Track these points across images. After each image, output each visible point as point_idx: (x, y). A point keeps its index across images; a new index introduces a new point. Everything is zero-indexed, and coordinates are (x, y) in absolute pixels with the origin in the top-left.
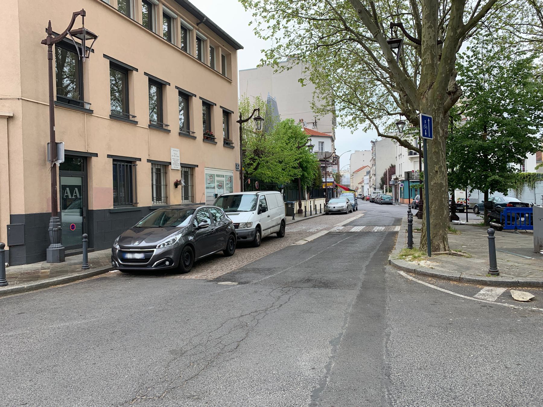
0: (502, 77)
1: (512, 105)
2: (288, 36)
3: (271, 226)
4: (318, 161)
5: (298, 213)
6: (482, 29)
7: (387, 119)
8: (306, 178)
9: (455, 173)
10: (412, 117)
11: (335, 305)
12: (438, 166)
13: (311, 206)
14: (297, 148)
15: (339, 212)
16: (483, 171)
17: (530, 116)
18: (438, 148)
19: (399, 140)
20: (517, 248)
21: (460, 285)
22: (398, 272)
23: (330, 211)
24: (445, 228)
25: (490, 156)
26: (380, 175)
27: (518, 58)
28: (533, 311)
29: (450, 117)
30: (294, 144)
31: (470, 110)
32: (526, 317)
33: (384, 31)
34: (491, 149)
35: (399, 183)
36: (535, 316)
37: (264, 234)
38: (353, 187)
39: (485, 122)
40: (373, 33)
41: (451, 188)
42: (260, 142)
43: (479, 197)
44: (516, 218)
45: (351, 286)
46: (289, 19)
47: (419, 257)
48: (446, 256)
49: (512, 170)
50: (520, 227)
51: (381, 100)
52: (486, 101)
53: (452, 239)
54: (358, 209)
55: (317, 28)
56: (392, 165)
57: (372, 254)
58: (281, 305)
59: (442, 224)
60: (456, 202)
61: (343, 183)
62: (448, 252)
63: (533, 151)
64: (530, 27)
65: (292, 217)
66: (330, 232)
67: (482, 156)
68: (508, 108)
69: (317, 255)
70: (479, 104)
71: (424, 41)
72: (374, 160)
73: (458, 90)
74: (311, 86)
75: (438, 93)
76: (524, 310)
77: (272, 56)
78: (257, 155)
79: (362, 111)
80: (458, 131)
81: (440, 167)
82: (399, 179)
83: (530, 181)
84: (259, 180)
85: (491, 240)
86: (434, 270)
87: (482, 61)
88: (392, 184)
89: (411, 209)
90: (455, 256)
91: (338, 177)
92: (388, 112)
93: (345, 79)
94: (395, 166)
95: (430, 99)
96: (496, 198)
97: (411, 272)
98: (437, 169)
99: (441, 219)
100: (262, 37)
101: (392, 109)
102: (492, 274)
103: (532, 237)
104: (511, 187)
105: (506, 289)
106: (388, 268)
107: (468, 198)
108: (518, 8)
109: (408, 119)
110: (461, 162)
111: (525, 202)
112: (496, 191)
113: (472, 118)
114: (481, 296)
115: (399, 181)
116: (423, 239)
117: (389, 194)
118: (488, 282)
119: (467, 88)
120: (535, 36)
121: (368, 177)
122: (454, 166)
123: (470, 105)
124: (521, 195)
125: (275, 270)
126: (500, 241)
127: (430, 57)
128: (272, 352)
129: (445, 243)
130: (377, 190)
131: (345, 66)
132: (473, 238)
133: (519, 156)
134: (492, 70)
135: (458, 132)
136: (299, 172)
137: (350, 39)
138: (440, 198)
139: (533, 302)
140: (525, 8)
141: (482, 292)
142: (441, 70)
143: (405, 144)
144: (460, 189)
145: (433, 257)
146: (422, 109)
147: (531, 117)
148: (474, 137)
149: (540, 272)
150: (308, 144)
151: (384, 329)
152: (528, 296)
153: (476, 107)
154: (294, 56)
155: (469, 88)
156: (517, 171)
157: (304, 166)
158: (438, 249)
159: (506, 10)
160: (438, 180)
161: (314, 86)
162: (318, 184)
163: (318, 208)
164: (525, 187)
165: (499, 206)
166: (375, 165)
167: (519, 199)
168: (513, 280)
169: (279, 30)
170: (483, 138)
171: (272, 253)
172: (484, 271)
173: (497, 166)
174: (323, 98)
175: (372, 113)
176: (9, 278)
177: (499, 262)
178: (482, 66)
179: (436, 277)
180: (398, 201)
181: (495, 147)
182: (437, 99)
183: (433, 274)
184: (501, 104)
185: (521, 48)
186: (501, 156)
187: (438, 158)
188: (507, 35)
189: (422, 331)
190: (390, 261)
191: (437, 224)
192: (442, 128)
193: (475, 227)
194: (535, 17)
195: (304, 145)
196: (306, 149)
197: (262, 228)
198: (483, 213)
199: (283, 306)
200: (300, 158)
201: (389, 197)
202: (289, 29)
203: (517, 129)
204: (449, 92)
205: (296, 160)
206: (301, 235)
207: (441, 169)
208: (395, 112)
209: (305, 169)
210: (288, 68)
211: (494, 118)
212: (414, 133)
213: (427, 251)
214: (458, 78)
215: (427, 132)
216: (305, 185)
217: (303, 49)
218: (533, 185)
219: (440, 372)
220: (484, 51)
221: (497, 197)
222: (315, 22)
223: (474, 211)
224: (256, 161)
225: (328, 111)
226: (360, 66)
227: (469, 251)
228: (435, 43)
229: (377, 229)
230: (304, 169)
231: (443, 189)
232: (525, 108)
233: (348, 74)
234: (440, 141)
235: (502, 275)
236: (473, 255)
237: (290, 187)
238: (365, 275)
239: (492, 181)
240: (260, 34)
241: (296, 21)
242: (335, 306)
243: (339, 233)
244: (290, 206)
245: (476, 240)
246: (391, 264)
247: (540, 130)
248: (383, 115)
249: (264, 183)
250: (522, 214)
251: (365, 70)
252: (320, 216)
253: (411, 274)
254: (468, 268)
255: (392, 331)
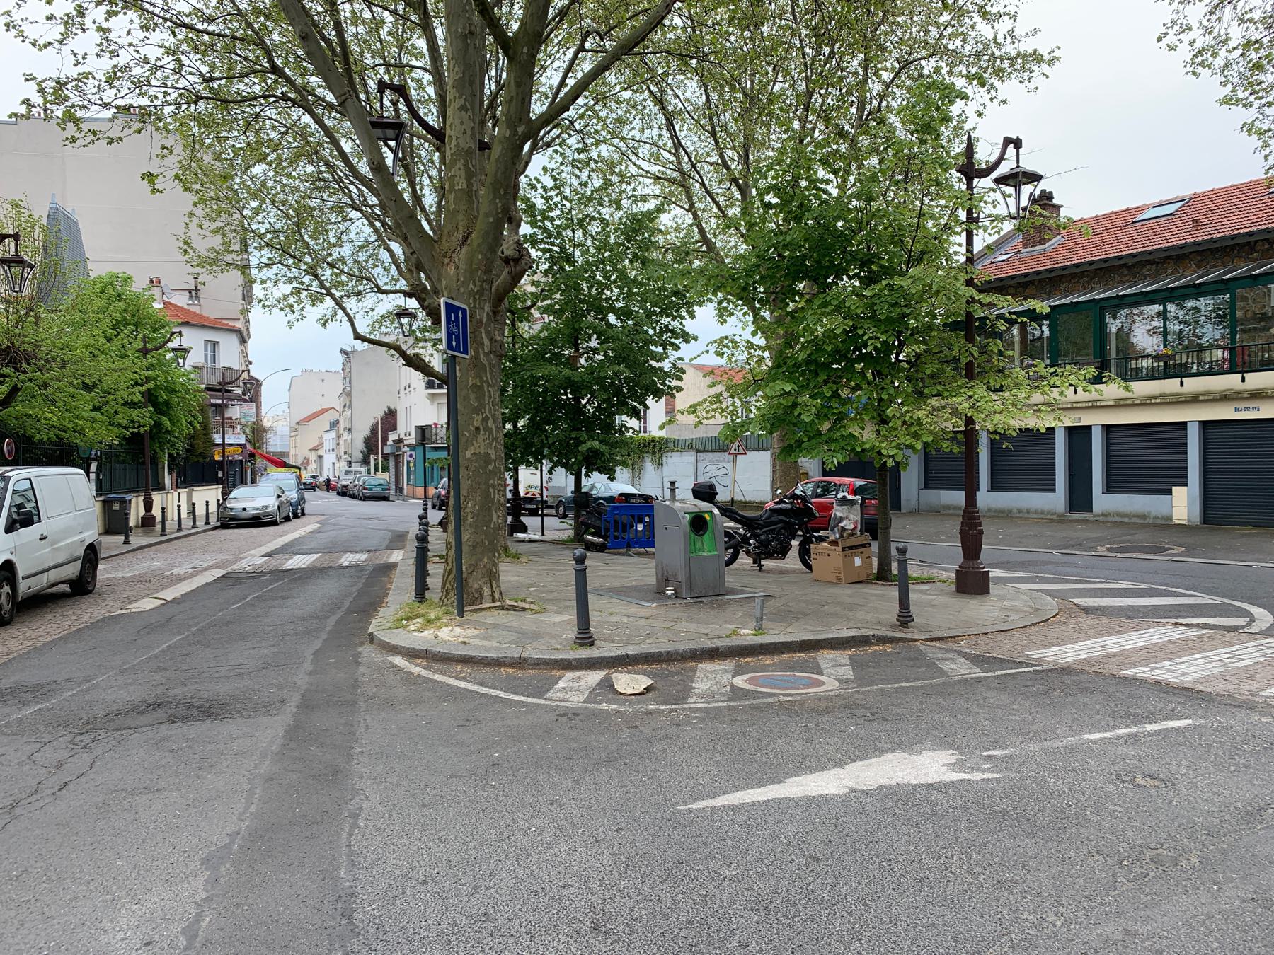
0: (606, 242)
2: (111, 52)
3: (52, 564)
4: (202, 391)
5: (143, 526)
6: (570, 136)
8: (168, 432)
11: (226, 759)
13: (179, 506)
14: (139, 351)
15: (258, 521)
18: (481, 378)
19: (403, 354)
21: (520, 674)
22: (389, 658)
23: (233, 518)
25: (586, 400)
26: (362, 431)
27: (635, 209)
28: (649, 713)
30: (131, 340)
32: (636, 727)
33: (368, 98)
37: (23, 587)
38: (296, 458)
40: (338, 94)
42: (22, 328)
45: (267, 708)
46: (114, 8)
47: (438, 619)
48: (495, 612)
50: (636, 543)
51: (362, 257)
52: (578, 288)
53: (509, 574)
54: (306, 512)
55: (196, 50)
56: (389, 408)
57: (332, 621)
58: (66, 784)
60: (522, 494)
61: (272, 449)
62: (498, 604)
63: (658, 394)
64: (655, 149)
65: (122, 538)
66: (230, 573)
69: (188, 636)
70: (564, 291)
71: (450, 136)
72: (349, 395)
74: (178, 201)
76: (634, 713)
77: (60, 98)
78: (10, 362)
79: (316, 276)
80: (525, 344)
81: (485, 420)
82: (406, 443)
83: (654, 453)
84: (17, 434)
87: (570, 201)
91: (257, 433)
92: (377, 286)
93: (273, 192)
96: (598, 486)
97: (418, 657)
100: (27, 41)
101: (387, 280)
102: (581, 645)
103: (651, 563)
104: (624, 464)
106: (367, 651)
108: (634, 107)
109: (423, 307)
111: (646, 492)
113: (551, 318)
117: (382, 477)
120: (663, 169)
121: (333, 434)
122: (519, 418)
125: (54, 687)
127: (463, 173)
128: (22, 925)
129: (494, 584)
130: (356, 467)
131: (272, 161)
134: (588, 224)
136: (144, 417)
137: (284, 97)
138: (483, 487)
139: (650, 695)
140: (647, 111)
141: (561, 684)
142: (485, 207)
143: (415, 363)
145: (469, 616)
148: (557, 357)
150: (174, 343)
151: (346, 802)
152: (643, 682)
153: (558, 296)
154: (128, 110)
155: (547, 255)
157: (160, 399)
158: (478, 599)
159: (614, 108)
161: (190, 198)
162: (200, 448)
163: (200, 511)
166: (350, 406)
168: (619, 653)
169: (84, 31)
170: (573, 362)
171: (49, 639)
172: (566, 639)
174: (216, 231)
175: (339, 284)
177: (594, 616)
178: (570, 211)
180: (401, 492)
184: (604, 297)
185: (639, 188)
187: (480, 398)
188: (616, 157)
189: (434, 792)
190: (372, 633)
192: (488, 333)
193: (559, 546)
194: (664, 132)
195: (161, 347)
196: (167, 357)
197: (21, 572)
198: (571, 515)
199: (71, 787)
200: (148, 379)
201: (382, 482)
202: (113, 36)
203: (631, 349)
204: (507, 257)
205: (136, 384)
206: (148, 584)
208: (393, 288)
209: (165, 409)
210: (108, 138)
214: (525, 229)
215: (457, 342)
216: (162, 450)
217: (156, 97)
219: (467, 880)
220: (575, 182)
221: (598, 484)
222: (190, 35)
223: (557, 511)
224: (7, 380)
225: (228, 264)
226: (310, 169)
227: (542, 599)
228: (473, 145)
229: (349, 559)
230: (162, 408)
231: (490, 467)
232: (645, 308)
233: (280, 181)
236: (547, 607)
237: (117, 456)
238: (310, 674)
240: (22, 31)
241: (137, 21)
242: (224, 765)
243: (255, 575)
244: (116, 507)
249: (34, 443)
251: (323, 179)
252: (205, 531)
253: (419, 661)
254: (536, 636)
255: (364, 805)
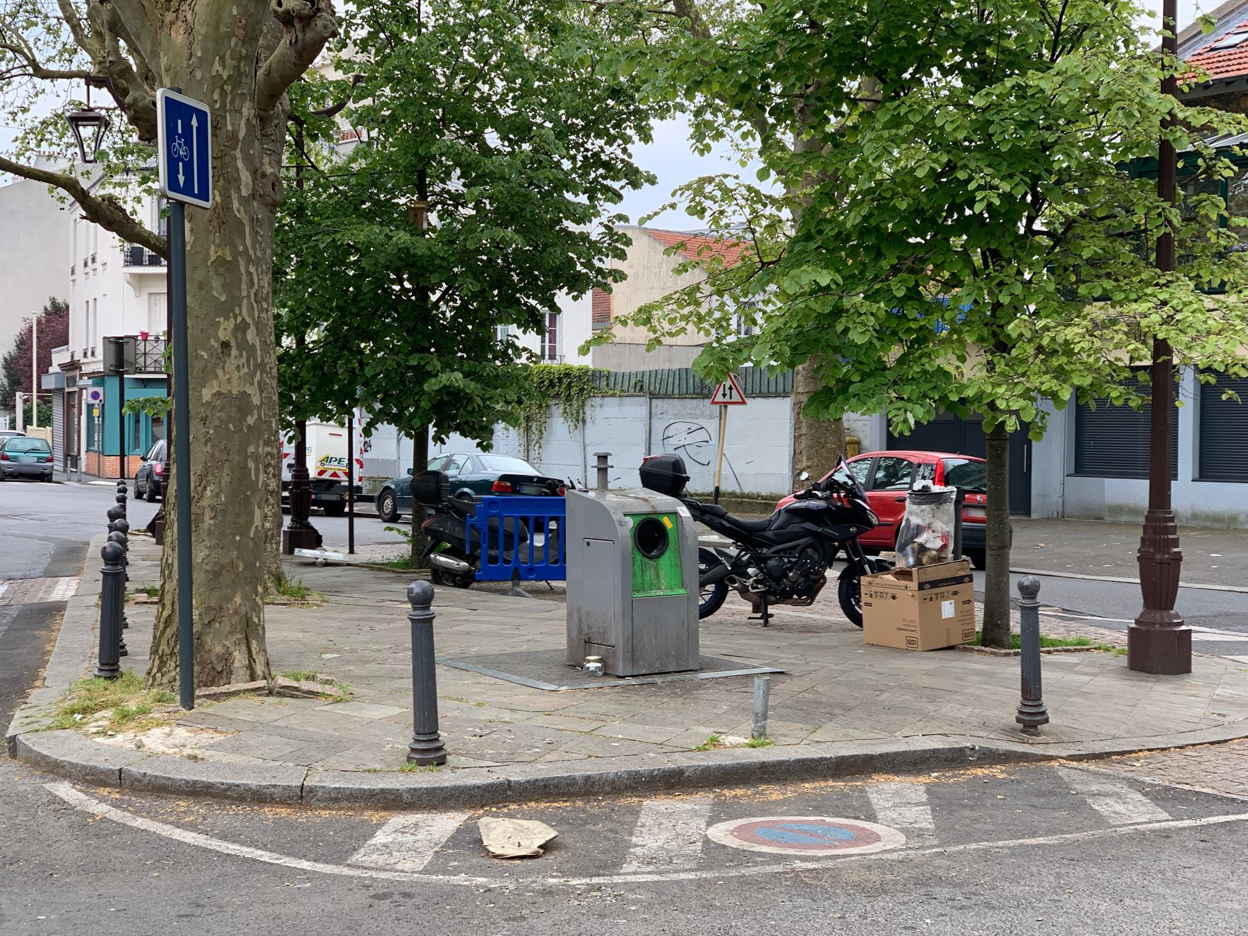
1: (513, 104)
7: (32, 92)
9: (309, 356)
10: (135, 100)
12: (232, 321)
16: (410, 353)
17: (572, 152)
18: (234, 247)
19: (82, 197)
20: (513, 650)
22: (47, 786)
24: (255, 580)
25: (438, 294)
28: (548, 892)
29: (290, 118)
31: (368, 102)
32: (523, 918)
34: (440, 267)
35: (81, 383)
36: (553, 911)
39: (421, 159)
41: (291, 414)
43: (399, 452)
44: (516, 540)
47: (143, 712)
48: (255, 700)
49: (510, 351)
50: (531, 570)
52: (425, 77)
56: (53, 301)
59: (241, 567)
60: (313, 474)
62: (261, 683)
63: (577, 285)
67: (408, 290)
68: (501, 111)
70: (399, 81)
73: (319, 10)
75: (235, 12)
76: (519, 892)
80: (323, 182)
81: (242, 328)
82: (85, 369)
83: (569, 398)
85: (419, 625)
86: (199, 766)
88: (52, 386)
89: (129, 504)
90: (292, 696)
92: (33, 63)
94: (67, 307)
95: (203, 32)
96: (459, 460)
97: (104, 784)
98: (229, 332)
99: (239, 547)
101: (53, 53)
102: (422, 763)
105: (466, 817)
107: (356, 456)
109: (121, 106)
110: (332, 310)
111: (553, 472)
112: (455, 430)
113: (374, 133)
114: (375, 856)
115: (82, 376)
116: (163, 632)
117: (39, 435)
118: (405, 796)
119: (359, 9)
122: (307, 325)
123: (370, 79)
124: (540, 447)
126: (461, 628)
129: (254, 645)
132: (368, 620)
133: (533, 302)
135: (321, 186)
141: (380, 838)
144: (328, 420)
145: (203, 707)
146: (167, 71)
147: (573, 158)
148: (383, 211)
149: (581, 738)
152: (537, 833)
153: (387, 91)
156: (525, 355)
158: (221, 673)
160: (229, 380)
164: (554, 419)
165: (466, 490)
167: (532, 465)
170: (412, 220)
173: (459, 334)
176: (704, 816)
177: (445, 708)
179: (206, 794)
181: (453, 259)
182: (230, 36)
183: (195, 782)
184: (477, 95)
186: (474, 296)
187: (231, 287)
190: (13, 739)
191: (222, 567)
192: (248, 160)
193: (384, 575)
198: (407, 514)
201: (38, 445)
203: (527, 198)
204: (287, 12)
207: (244, 333)
208: (65, 68)
211: (452, 146)
212: (147, 169)
213: (178, 683)
218: (578, 413)
223: (380, 507)
227: (349, 677)
231: (250, 420)
232: (556, 121)
234: (242, 215)
235: (456, 763)
236: (357, 691)
239: (439, 391)
245: (378, 627)
246: (20, 753)
247: (599, 208)
248: (14, 72)
250: (537, 519)
253: (104, 791)
254: (334, 746)
